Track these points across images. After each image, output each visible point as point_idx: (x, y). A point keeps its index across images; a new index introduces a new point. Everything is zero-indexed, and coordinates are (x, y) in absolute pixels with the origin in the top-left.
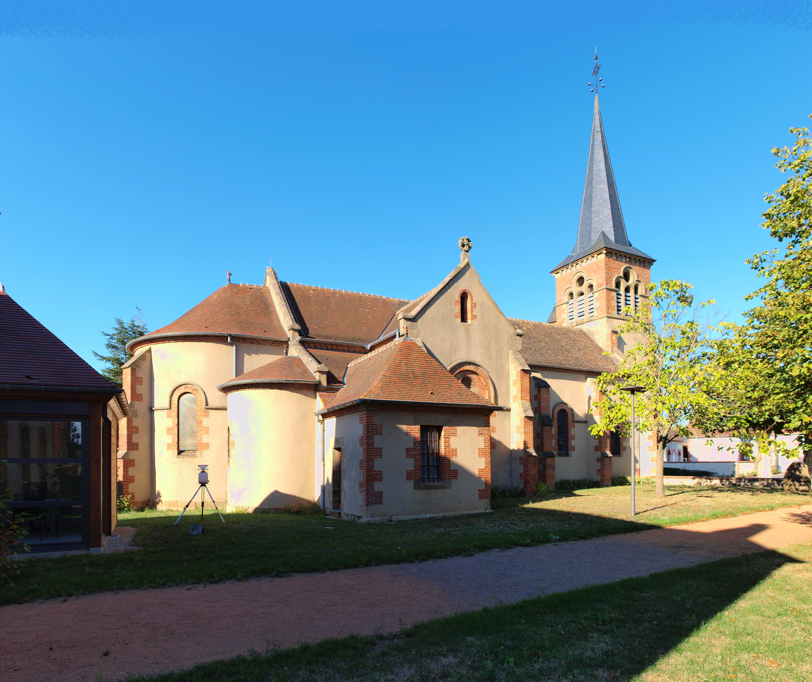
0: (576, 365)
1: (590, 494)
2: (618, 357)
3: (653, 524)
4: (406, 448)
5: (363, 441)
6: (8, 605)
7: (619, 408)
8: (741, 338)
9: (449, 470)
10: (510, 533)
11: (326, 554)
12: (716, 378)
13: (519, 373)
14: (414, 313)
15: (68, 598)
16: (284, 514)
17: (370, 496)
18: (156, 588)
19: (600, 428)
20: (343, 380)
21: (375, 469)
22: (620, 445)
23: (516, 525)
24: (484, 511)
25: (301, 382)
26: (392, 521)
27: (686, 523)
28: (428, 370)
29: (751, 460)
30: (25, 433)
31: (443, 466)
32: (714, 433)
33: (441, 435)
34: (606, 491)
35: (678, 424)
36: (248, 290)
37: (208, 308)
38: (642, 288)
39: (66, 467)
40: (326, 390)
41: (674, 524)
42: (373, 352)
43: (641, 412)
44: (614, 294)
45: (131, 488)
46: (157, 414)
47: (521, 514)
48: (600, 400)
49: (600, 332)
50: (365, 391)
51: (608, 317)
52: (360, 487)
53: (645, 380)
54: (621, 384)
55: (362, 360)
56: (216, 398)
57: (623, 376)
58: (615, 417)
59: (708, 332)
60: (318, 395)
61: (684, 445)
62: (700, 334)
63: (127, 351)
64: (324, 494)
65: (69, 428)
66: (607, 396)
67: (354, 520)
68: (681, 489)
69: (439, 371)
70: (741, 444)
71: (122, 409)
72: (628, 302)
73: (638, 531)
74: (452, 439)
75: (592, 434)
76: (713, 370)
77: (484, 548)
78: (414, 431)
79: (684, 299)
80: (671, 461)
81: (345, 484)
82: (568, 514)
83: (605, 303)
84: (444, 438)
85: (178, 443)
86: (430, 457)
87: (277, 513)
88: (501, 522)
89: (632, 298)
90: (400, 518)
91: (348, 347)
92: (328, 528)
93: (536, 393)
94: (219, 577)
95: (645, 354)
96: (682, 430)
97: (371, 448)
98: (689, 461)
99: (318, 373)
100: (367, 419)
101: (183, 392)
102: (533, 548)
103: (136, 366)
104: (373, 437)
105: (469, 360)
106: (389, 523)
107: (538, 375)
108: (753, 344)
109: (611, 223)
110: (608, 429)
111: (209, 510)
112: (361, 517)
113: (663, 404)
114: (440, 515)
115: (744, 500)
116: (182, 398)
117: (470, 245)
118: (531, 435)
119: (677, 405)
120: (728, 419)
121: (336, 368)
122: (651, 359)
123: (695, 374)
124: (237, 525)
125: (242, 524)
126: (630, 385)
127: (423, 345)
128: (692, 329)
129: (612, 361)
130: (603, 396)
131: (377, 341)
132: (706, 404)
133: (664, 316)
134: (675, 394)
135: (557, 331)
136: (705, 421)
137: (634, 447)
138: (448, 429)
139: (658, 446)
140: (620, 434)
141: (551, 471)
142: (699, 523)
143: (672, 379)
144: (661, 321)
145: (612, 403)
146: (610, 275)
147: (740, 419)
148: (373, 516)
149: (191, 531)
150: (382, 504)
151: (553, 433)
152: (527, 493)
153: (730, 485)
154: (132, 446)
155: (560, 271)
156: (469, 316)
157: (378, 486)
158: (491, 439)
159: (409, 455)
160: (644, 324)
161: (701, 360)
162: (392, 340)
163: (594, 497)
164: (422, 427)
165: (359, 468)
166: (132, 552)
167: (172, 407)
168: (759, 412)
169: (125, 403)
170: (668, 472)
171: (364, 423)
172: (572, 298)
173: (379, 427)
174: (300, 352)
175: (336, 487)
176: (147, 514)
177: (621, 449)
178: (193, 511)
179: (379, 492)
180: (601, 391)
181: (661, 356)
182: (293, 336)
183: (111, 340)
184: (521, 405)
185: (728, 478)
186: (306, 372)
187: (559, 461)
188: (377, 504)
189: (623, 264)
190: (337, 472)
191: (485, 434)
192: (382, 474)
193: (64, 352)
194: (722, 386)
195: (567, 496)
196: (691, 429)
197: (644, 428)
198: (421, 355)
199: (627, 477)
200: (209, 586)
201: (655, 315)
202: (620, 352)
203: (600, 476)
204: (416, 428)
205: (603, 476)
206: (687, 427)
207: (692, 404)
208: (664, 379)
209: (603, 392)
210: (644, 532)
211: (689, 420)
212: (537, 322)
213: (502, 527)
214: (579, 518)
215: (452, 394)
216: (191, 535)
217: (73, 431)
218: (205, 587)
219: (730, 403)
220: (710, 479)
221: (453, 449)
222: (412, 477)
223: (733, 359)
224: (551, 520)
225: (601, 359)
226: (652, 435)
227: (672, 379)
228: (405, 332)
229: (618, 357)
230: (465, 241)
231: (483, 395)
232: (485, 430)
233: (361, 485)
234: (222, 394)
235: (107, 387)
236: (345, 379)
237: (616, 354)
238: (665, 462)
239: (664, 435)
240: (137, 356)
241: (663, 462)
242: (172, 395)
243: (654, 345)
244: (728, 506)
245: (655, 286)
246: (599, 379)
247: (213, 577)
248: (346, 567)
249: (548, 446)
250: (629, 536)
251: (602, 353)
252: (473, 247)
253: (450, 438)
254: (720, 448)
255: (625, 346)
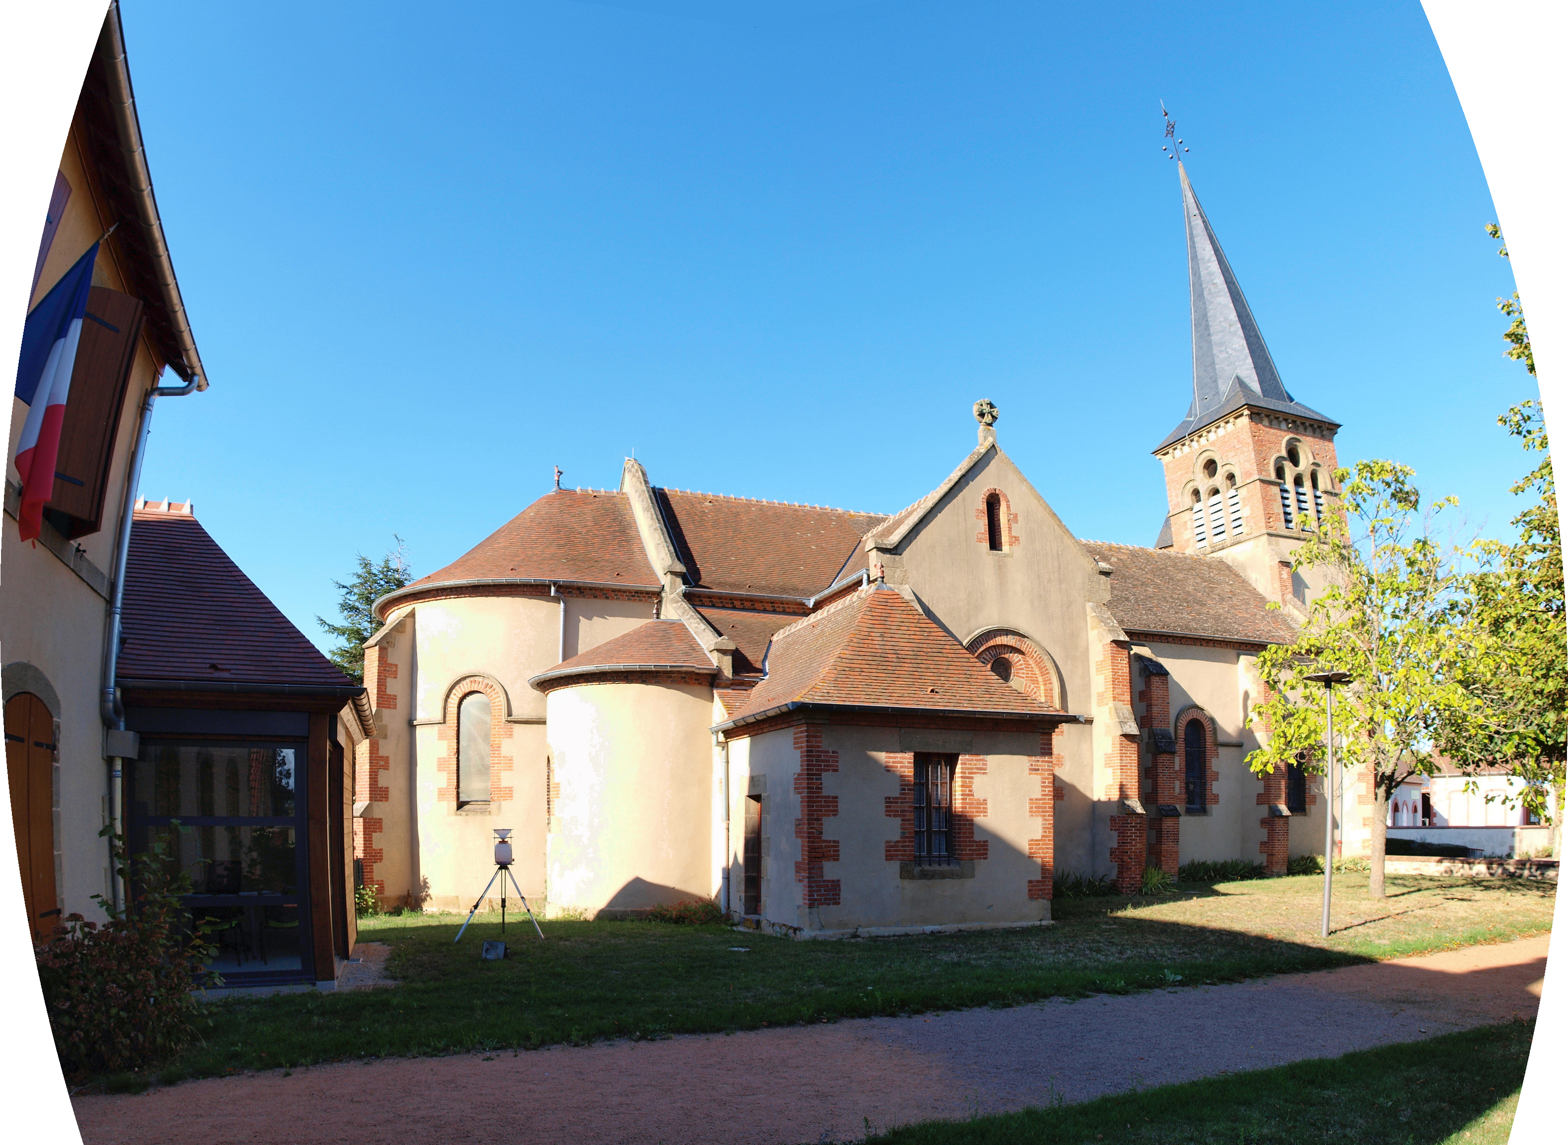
0: (1217, 630)
1: (1245, 892)
2: (1296, 613)
3: (1361, 954)
4: (886, 798)
5: (800, 784)
6: (203, 1078)
7: (1302, 717)
8: (1515, 568)
9: (970, 842)
10: (1086, 968)
11: (734, 999)
12: (1478, 653)
13: (1108, 648)
14: (895, 538)
15: (293, 1069)
16: (653, 923)
17: (815, 888)
18: (432, 1056)
19: (1267, 758)
20: (764, 665)
21: (824, 837)
22: (1305, 793)
23: (1099, 951)
24: (1038, 923)
25: (684, 669)
26: (859, 937)
27: (1420, 952)
28: (925, 646)
29: (1543, 822)
30: (206, 765)
31: (959, 833)
32: (1478, 766)
33: (954, 773)
34: (1276, 885)
35: (1414, 748)
36: (591, 499)
37: (518, 535)
38: (1324, 478)
39: (270, 832)
40: (732, 684)
41: (1398, 954)
42: (820, 611)
43: (1344, 724)
44: (1276, 490)
45: (379, 871)
46: (421, 733)
47: (1110, 930)
48: (1267, 701)
49: (1256, 560)
50: (804, 688)
51: (1269, 535)
52: (797, 872)
53: (1349, 659)
54: (1305, 668)
55: (799, 627)
56: (526, 701)
57: (1309, 651)
58: (1296, 736)
59: (1455, 561)
60: (715, 695)
61: (1424, 791)
62: (1440, 564)
63: (374, 615)
64: (729, 885)
65: (274, 761)
66: (1280, 692)
67: (786, 935)
68: (1415, 883)
69: (947, 647)
70: (1527, 790)
71: (363, 725)
72: (1303, 505)
73: (1330, 968)
74: (978, 779)
75: (1252, 769)
76: (1472, 637)
77: (1036, 995)
78: (903, 763)
79: (1404, 497)
80: (1400, 825)
81: (769, 866)
82: (1202, 931)
83: (1261, 507)
84: (962, 777)
85: (458, 787)
86: (934, 815)
87: (640, 920)
88: (1071, 944)
89: (1309, 497)
90: (874, 931)
91: (772, 603)
92: (736, 949)
93: (1143, 688)
94: (540, 1038)
95: (1346, 606)
96: (1421, 761)
97: (817, 797)
98: (1432, 826)
99: (715, 653)
100: (808, 741)
101: (467, 691)
102: (1130, 998)
103: (388, 643)
104: (820, 775)
105: (1006, 626)
106: (853, 941)
107: (1144, 651)
108: (1540, 583)
109: (1250, 360)
110: (1282, 760)
111: (514, 915)
112: (800, 929)
113: (1385, 708)
114: (951, 927)
115: (1528, 907)
116: (465, 702)
117: (994, 414)
118: (1134, 772)
119: (1410, 709)
120: (1504, 737)
121: (749, 642)
122: (1358, 616)
123: (1440, 647)
124: (567, 943)
125: (576, 941)
126: (1323, 670)
127: (914, 598)
128: (1425, 555)
129: (1285, 622)
130: (1273, 692)
131: (827, 592)
132: (1464, 709)
133: (1372, 531)
134: (1407, 687)
135: (1176, 563)
136: (1462, 742)
137: (1333, 796)
138: (968, 760)
139: (1376, 795)
140: (1306, 769)
141: (1171, 844)
142: (1443, 954)
143: (1399, 657)
144: (1367, 540)
145: (1289, 706)
146: (1263, 455)
147: (1525, 738)
148: (822, 928)
149: (484, 954)
150: (838, 903)
151: (1177, 768)
152: (1123, 887)
153: (1504, 876)
154: (378, 793)
155: (1171, 451)
156: (1005, 538)
157: (830, 870)
158: (1054, 780)
159: (890, 811)
160: (1338, 546)
161: (1448, 616)
162: (855, 590)
163: (1253, 897)
164: (917, 756)
165: (794, 835)
166: (387, 991)
167: (447, 719)
168: (1557, 722)
169: (368, 712)
170: (1394, 847)
171: (801, 748)
172: (1199, 500)
173: (831, 757)
174: (683, 613)
175: (751, 870)
176: (407, 920)
177: (1307, 800)
178: (487, 915)
179: (833, 881)
180: (1267, 682)
181: (1376, 609)
182: (673, 584)
183: (348, 596)
184: (1113, 712)
185: (1501, 861)
186: (694, 650)
187: (1188, 824)
188: (829, 904)
189: (1283, 433)
190: (754, 844)
191: (1042, 770)
192: (838, 846)
193: (273, 621)
194: (1491, 670)
195: (1200, 896)
196: (1437, 760)
197: (1351, 758)
198: (911, 617)
199: (1317, 856)
200: (524, 1055)
201: (1355, 529)
202: (1299, 603)
203: (1265, 855)
204: (905, 758)
205: (1271, 855)
206: (1430, 756)
207: (1438, 707)
208: (1384, 656)
209: (1272, 685)
210: (1343, 969)
211: (1432, 741)
212: (1137, 547)
213: (1071, 955)
214: (1222, 939)
215: (973, 692)
216: (485, 961)
217: (280, 765)
218: (516, 1056)
219: (1505, 704)
220: (1469, 863)
221: (978, 799)
222: (897, 855)
223: (1505, 613)
224: (1169, 944)
225: (1263, 617)
226: (1365, 771)
227: (1399, 657)
228: (879, 575)
229: (1296, 613)
230: (984, 407)
231: (1035, 693)
232: (1043, 761)
233: (798, 867)
234: (537, 693)
235: (338, 684)
236: (767, 663)
237: (1290, 606)
238: (1388, 828)
239: (1388, 772)
240: (391, 624)
241: (1385, 828)
242: (448, 696)
243: (1360, 587)
244: (1498, 920)
245: (1348, 474)
246: (1262, 659)
247: (528, 1038)
248: (771, 1024)
249: (1166, 793)
250: (1314, 976)
251: (1265, 605)
252: (999, 418)
253: (972, 778)
254: (1489, 798)
255: (1306, 590)
